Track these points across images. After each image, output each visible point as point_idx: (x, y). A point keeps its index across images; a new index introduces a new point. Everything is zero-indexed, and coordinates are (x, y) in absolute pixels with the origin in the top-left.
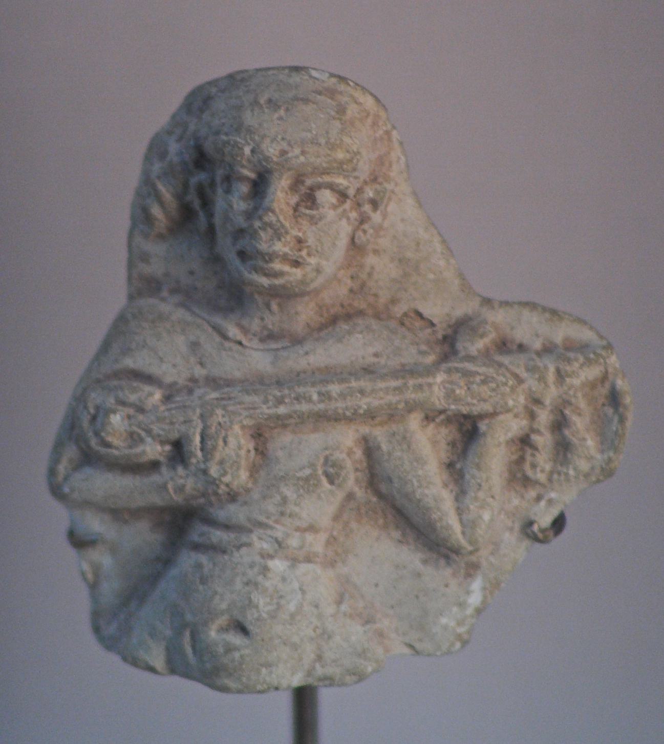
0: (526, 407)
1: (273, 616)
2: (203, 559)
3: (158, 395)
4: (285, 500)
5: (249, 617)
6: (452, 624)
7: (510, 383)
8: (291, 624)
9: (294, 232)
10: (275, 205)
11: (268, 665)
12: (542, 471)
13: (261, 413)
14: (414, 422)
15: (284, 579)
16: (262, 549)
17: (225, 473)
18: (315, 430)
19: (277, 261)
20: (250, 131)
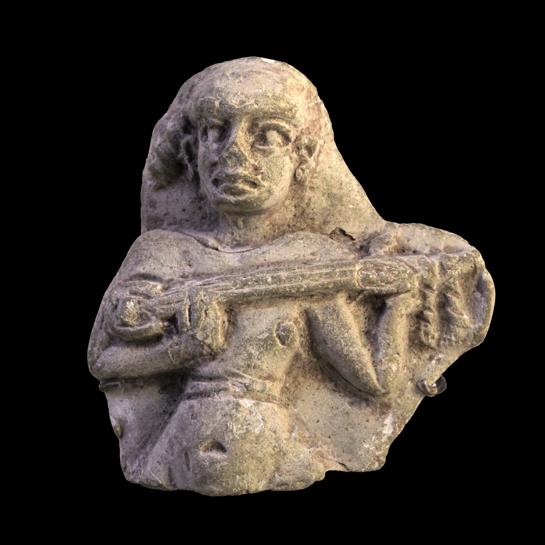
0: (420, 291)
1: (243, 437)
2: (194, 402)
3: (159, 287)
4: (250, 355)
5: (227, 439)
6: (372, 448)
7: (408, 271)
9: (252, 161)
10: (237, 140)
11: (241, 473)
12: (433, 338)
13: (232, 293)
14: (341, 300)
16: (235, 392)
17: (206, 338)
18: (270, 305)
19: (240, 181)
20: (219, 91)
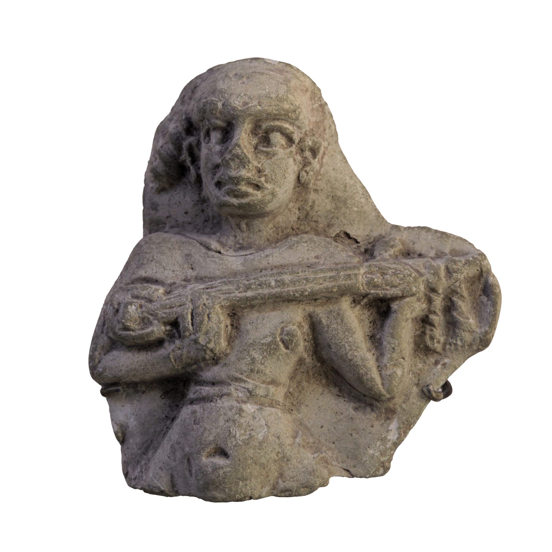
1: (246, 443)
2: (196, 407)
3: (161, 290)
4: (253, 360)
5: (230, 445)
6: (377, 454)
7: (413, 275)
8: (260, 449)
9: (255, 163)
11: (244, 479)
12: (439, 342)
13: (235, 297)
14: (345, 304)
15: (254, 418)
16: (238, 397)
17: (209, 342)
18: (274, 309)
19: (243, 183)
20: (221, 92)
